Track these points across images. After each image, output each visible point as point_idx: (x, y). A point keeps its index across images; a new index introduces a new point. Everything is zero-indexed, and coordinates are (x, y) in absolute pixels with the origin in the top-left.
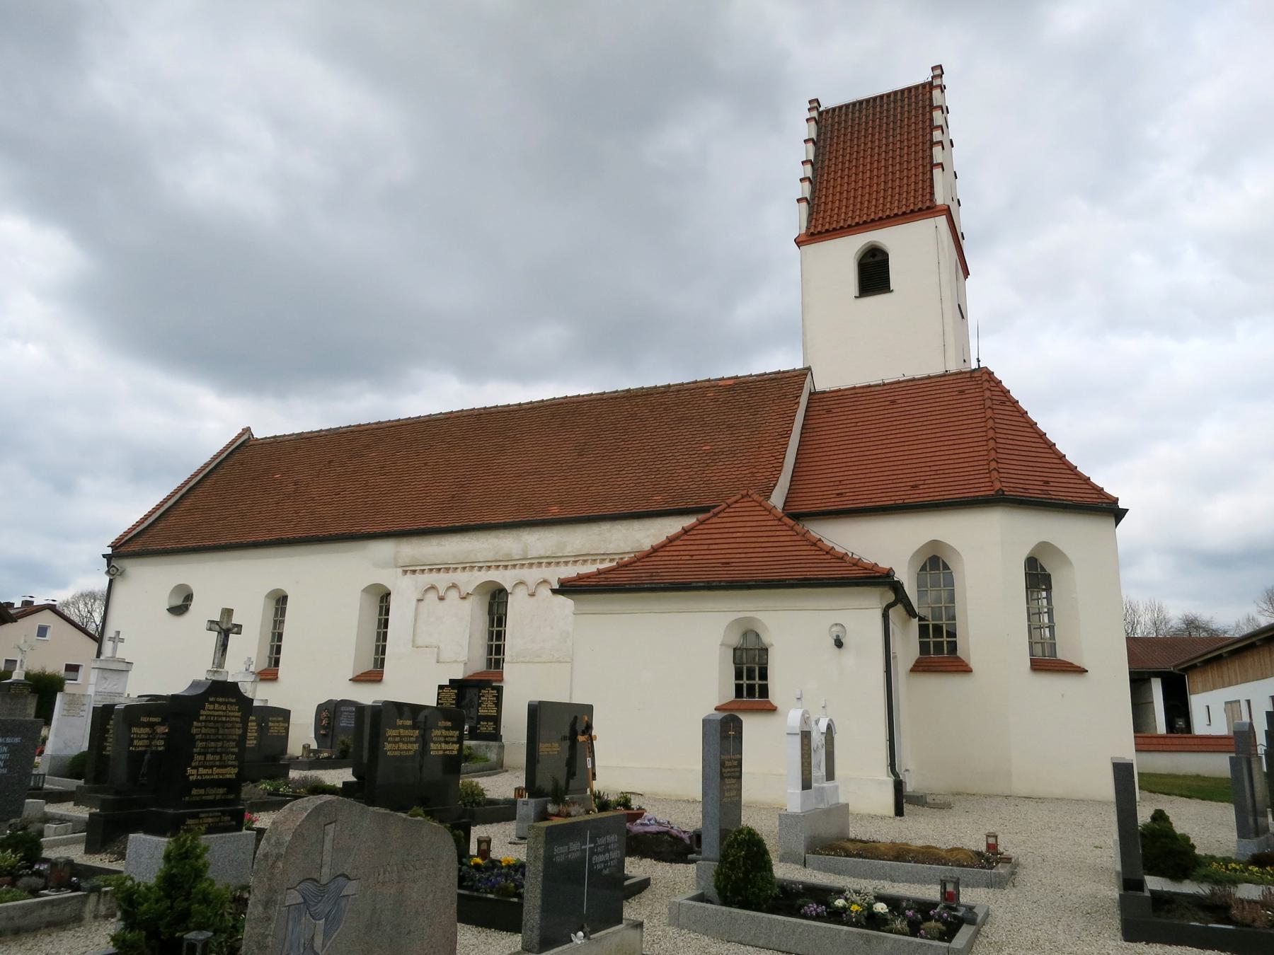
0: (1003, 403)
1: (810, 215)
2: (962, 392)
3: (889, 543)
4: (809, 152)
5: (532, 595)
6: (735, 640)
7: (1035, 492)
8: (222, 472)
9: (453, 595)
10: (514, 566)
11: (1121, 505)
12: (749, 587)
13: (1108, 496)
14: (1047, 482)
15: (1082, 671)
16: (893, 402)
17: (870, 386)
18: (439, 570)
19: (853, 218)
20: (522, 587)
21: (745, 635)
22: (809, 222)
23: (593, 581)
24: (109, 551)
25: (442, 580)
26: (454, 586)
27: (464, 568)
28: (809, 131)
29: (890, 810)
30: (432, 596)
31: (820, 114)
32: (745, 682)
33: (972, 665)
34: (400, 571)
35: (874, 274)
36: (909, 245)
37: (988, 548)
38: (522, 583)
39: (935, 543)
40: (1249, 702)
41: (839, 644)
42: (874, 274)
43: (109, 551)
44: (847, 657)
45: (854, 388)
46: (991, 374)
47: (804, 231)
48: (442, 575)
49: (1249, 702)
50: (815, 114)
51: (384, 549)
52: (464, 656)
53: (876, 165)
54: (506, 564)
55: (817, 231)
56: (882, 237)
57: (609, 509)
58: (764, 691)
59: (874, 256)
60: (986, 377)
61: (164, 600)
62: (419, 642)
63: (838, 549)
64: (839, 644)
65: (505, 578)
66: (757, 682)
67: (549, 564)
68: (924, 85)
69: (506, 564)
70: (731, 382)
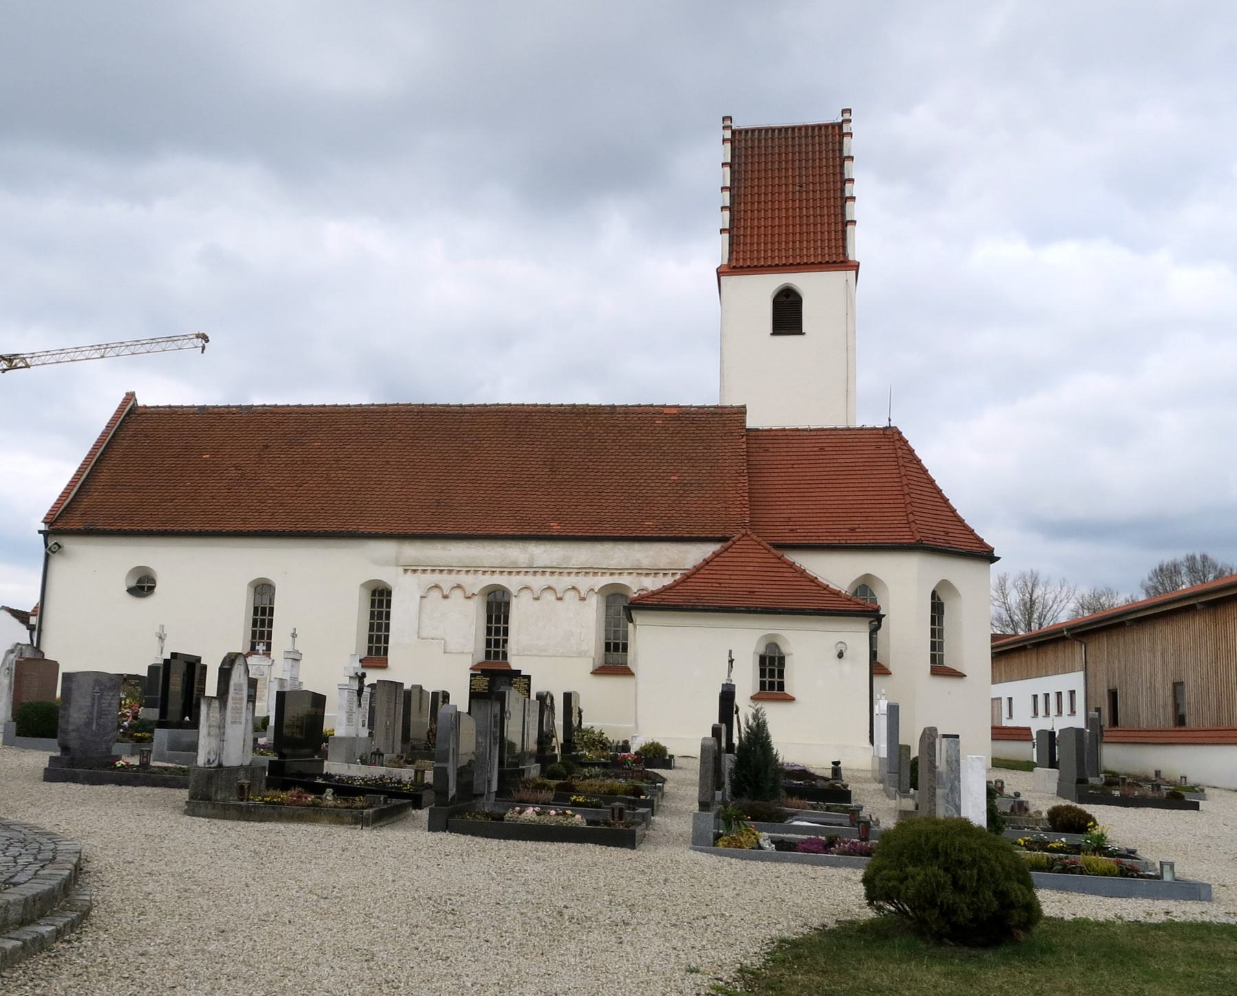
0: (910, 461)
1: (731, 244)
2: (878, 447)
3: (837, 571)
4: (725, 177)
5: (537, 599)
6: (762, 650)
7: (940, 543)
8: (125, 443)
9: (458, 594)
10: (518, 573)
11: (996, 554)
12: (780, 613)
13: (987, 546)
14: (947, 533)
15: (962, 676)
16: (822, 449)
17: (797, 430)
18: (441, 571)
19: (773, 258)
20: (551, 592)
21: (767, 646)
22: (731, 253)
23: (654, 601)
24: (43, 527)
25: (447, 581)
26: (459, 586)
27: (468, 572)
28: (725, 153)
29: (1170, 724)
30: (436, 594)
31: (733, 132)
32: (767, 679)
33: (891, 670)
34: (401, 569)
35: (787, 315)
36: (813, 287)
37: (904, 581)
38: (549, 588)
39: (868, 577)
40: (1010, 699)
41: (840, 655)
42: (787, 315)
43: (43, 527)
44: (845, 664)
45: (784, 430)
46: (900, 433)
47: (726, 262)
48: (445, 576)
49: (1010, 699)
50: (728, 134)
51: (387, 549)
52: (470, 647)
53: (788, 201)
54: (512, 570)
55: (739, 263)
56: (801, 281)
57: (607, 530)
58: (781, 686)
59: (787, 296)
60: (896, 437)
61: (121, 583)
62: (424, 634)
63: (831, 586)
64: (840, 655)
65: (511, 583)
66: (776, 679)
67: (552, 573)
68: (833, 126)
69: (512, 570)
70: (675, 411)
